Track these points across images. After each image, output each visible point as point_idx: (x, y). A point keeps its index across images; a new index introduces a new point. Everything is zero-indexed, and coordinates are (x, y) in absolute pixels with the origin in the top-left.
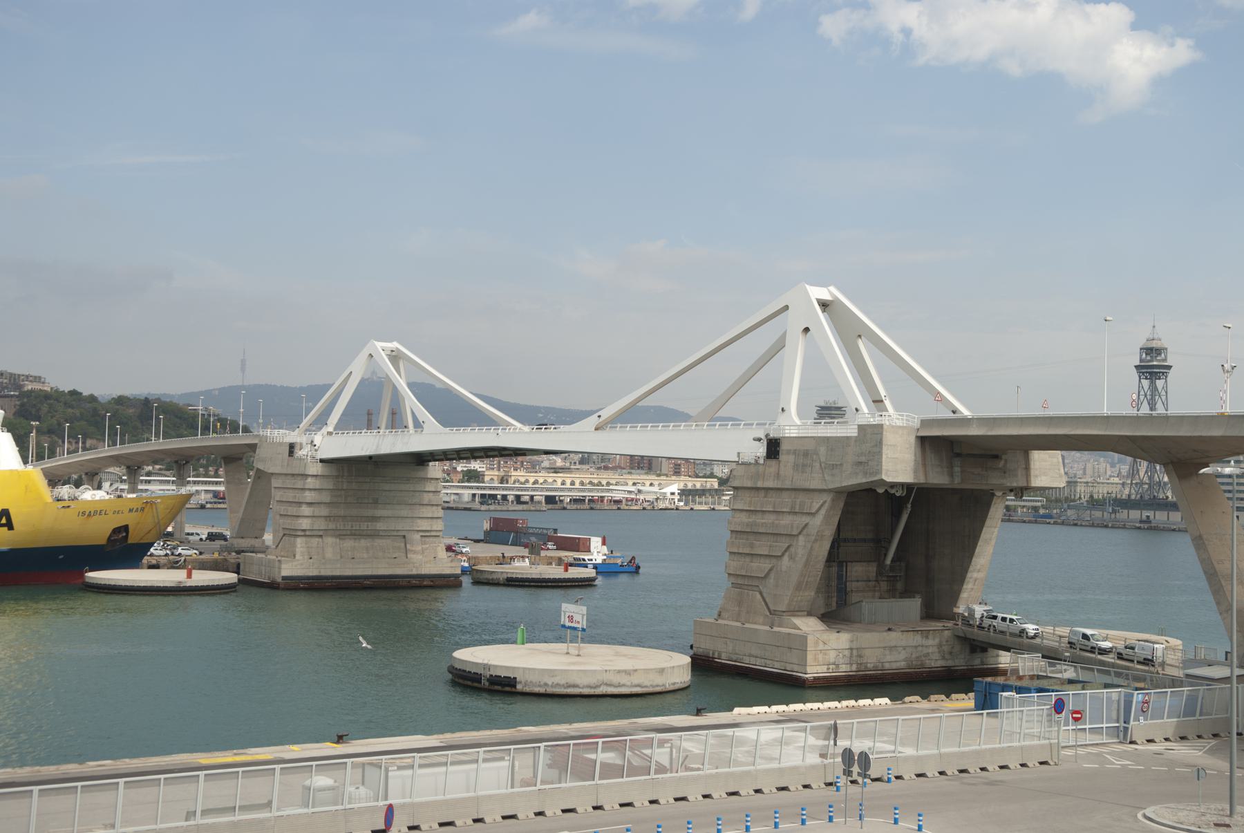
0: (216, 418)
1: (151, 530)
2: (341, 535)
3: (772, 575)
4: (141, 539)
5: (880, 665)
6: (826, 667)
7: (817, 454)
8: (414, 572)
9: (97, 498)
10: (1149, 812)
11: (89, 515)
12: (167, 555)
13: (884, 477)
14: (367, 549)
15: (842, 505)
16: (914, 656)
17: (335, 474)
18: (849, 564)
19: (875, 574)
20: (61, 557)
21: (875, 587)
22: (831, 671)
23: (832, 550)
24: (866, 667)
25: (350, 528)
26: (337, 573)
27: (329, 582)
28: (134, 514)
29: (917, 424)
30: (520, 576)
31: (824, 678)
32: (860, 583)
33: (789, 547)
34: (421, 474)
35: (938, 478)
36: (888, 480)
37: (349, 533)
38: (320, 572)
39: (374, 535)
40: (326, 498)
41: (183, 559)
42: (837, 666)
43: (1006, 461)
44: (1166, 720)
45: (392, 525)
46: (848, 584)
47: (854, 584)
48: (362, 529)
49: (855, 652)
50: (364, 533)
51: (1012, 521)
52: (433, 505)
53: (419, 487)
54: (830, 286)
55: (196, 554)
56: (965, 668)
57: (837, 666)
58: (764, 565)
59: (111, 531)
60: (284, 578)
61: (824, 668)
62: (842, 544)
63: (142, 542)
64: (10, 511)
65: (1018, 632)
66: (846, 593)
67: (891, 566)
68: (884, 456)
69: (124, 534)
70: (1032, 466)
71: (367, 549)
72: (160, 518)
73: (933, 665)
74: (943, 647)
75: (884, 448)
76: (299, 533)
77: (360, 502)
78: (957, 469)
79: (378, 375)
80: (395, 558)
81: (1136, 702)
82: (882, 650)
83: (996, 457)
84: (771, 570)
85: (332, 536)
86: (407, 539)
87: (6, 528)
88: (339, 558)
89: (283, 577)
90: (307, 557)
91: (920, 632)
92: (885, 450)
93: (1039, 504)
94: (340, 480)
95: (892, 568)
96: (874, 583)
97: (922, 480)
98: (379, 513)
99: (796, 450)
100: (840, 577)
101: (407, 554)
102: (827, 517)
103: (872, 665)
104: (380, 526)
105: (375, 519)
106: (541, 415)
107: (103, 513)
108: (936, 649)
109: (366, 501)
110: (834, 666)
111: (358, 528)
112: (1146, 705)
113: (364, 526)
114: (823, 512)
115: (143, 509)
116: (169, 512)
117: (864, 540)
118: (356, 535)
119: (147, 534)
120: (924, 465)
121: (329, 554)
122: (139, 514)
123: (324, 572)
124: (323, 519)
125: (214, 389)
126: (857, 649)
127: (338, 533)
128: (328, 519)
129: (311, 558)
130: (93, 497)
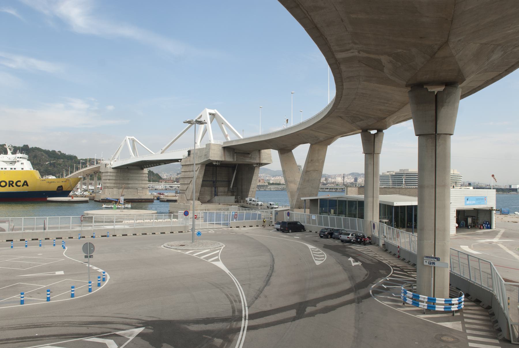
2: (119, 188)
3: (188, 189)
4: (67, 189)
7: (198, 154)
8: (140, 198)
9: (53, 178)
10: (165, 245)
11: (50, 183)
12: (81, 195)
14: (126, 192)
15: (204, 168)
17: (116, 172)
19: (227, 191)
20: (44, 194)
23: (380, 217)
28: (63, 183)
29: (222, 144)
30: (170, 199)
33: (191, 181)
34: (141, 172)
35: (229, 159)
36: (212, 159)
39: (128, 188)
40: (114, 178)
41: (85, 196)
43: (252, 155)
44: (244, 221)
45: (133, 185)
46: (218, 193)
47: (220, 193)
51: (337, 192)
52: (145, 180)
53: (141, 175)
54: (215, 109)
58: (185, 187)
60: (102, 199)
62: (217, 182)
64: (27, 181)
67: (232, 188)
68: (210, 152)
69: (61, 188)
70: (261, 157)
71: (126, 192)
72: (71, 184)
75: (211, 150)
76: (106, 187)
78: (235, 157)
81: (232, 215)
83: (249, 154)
84: (187, 188)
85: (116, 188)
87: (26, 186)
93: (343, 187)
95: (233, 188)
97: (223, 159)
98: (129, 182)
100: (215, 191)
102: (200, 172)
104: (130, 186)
105: (128, 184)
112: (236, 216)
114: (198, 170)
115: (66, 181)
117: (224, 181)
120: (224, 155)
121: (115, 193)
122: (65, 183)
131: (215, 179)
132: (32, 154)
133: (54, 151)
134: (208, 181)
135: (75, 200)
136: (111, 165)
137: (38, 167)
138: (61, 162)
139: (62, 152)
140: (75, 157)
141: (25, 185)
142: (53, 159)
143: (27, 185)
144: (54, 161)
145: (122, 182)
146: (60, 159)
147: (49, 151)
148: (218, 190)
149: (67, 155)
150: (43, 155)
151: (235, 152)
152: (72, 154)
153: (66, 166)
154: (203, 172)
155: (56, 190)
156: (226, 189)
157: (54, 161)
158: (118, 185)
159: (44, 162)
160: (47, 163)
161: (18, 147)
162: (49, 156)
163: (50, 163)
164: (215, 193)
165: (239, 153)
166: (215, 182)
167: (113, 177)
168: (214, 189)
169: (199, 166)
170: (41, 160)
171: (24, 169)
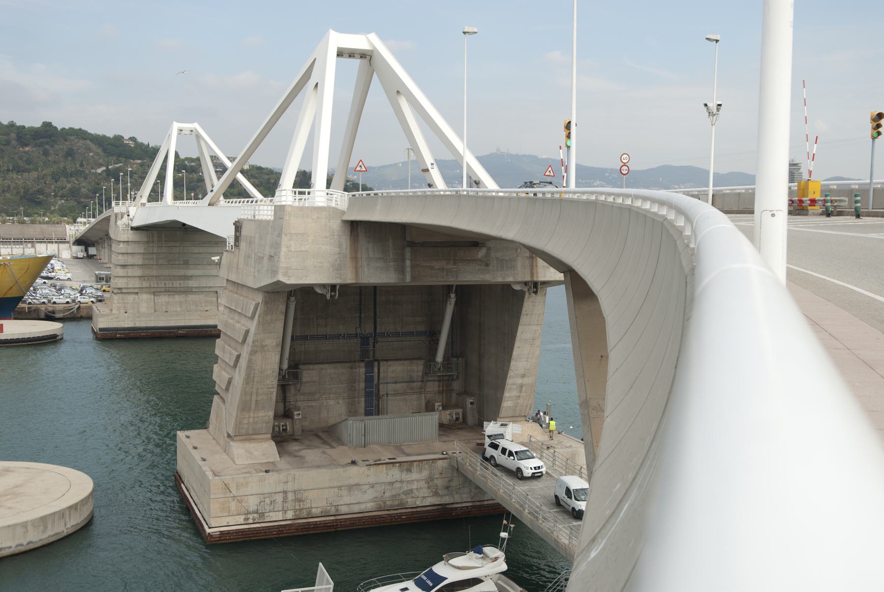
0: (351, 183)
1: (11, 288)
5: (333, 509)
6: (243, 517)
12: (68, 303)
14: (181, 303)
16: (388, 494)
17: (145, 239)
18: (381, 363)
19: (420, 374)
21: (421, 388)
22: (251, 521)
24: (310, 512)
25: (163, 286)
26: (152, 324)
31: (237, 532)
32: (399, 385)
36: (288, 282)
37: (163, 290)
38: (135, 324)
39: (187, 291)
40: (138, 260)
41: (77, 306)
42: (262, 515)
43: (489, 249)
45: (204, 283)
46: (381, 386)
47: (391, 387)
48: (174, 286)
49: (290, 496)
50: (178, 290)
54: (369, 33)
55: (92, 302)
56: (470, 504)
57: (262, 515)
61: (241, 519)
62: (380, 339)
63: (5, 297)
65: (514, 470)
66: (378, 397)
68: (284, 249)
73: (418, 503)
74: (435, 481)
77: (171, 263)
78: (408, 263)
79: (501, 151)
80: (207, 311)
82: (336, 490)
85: (147, 293)
86: (218, 294)
88: (153, 311)
89: (99, 328)
90: (123, 311)
91: (398, 465)
94: (151, 245)
96: (420, 383)
97: (348, 278)
98: (190, 272)
100: (369, 380)
103: (319, 510)
104: (192, 283)
105: (186, 278)
106: (607, 174)
108: (423, 484)
109: (177, 263)
110: (255, 515)
111: (172, 286)
113: (177, 284)
117: (411, 334)
119: (9, 290)
120: (355, 258)
121: (143, 308)
123: (139, 324)
124: (137, 278)
126: (295, 492)
127: (153, 290)
128: (142, 278)
129: (126, 312)
131: (368, 329)
132: (61, 147)
134: (338, 336)
136: (131, 217)
137: (78, 181)
139: (140, 140)
142: (115, 158)
145: (166, 272)
146: (134, 160)
148: (382, 375)
149: (152, 147)
150: (90, 150)
151: (408, 239)
156: (414, 368)
158: (154, 284)
159: (93, 168)
160: (99, 171)
161: (29, 127)
162: (105, 150)
163: (108, 170)
164: (366, 388)
165: (424, 244)
166: (371, 341)
167: (137, 256)
168: (362, 370)
169: (259, 298)
170: (84, 163)
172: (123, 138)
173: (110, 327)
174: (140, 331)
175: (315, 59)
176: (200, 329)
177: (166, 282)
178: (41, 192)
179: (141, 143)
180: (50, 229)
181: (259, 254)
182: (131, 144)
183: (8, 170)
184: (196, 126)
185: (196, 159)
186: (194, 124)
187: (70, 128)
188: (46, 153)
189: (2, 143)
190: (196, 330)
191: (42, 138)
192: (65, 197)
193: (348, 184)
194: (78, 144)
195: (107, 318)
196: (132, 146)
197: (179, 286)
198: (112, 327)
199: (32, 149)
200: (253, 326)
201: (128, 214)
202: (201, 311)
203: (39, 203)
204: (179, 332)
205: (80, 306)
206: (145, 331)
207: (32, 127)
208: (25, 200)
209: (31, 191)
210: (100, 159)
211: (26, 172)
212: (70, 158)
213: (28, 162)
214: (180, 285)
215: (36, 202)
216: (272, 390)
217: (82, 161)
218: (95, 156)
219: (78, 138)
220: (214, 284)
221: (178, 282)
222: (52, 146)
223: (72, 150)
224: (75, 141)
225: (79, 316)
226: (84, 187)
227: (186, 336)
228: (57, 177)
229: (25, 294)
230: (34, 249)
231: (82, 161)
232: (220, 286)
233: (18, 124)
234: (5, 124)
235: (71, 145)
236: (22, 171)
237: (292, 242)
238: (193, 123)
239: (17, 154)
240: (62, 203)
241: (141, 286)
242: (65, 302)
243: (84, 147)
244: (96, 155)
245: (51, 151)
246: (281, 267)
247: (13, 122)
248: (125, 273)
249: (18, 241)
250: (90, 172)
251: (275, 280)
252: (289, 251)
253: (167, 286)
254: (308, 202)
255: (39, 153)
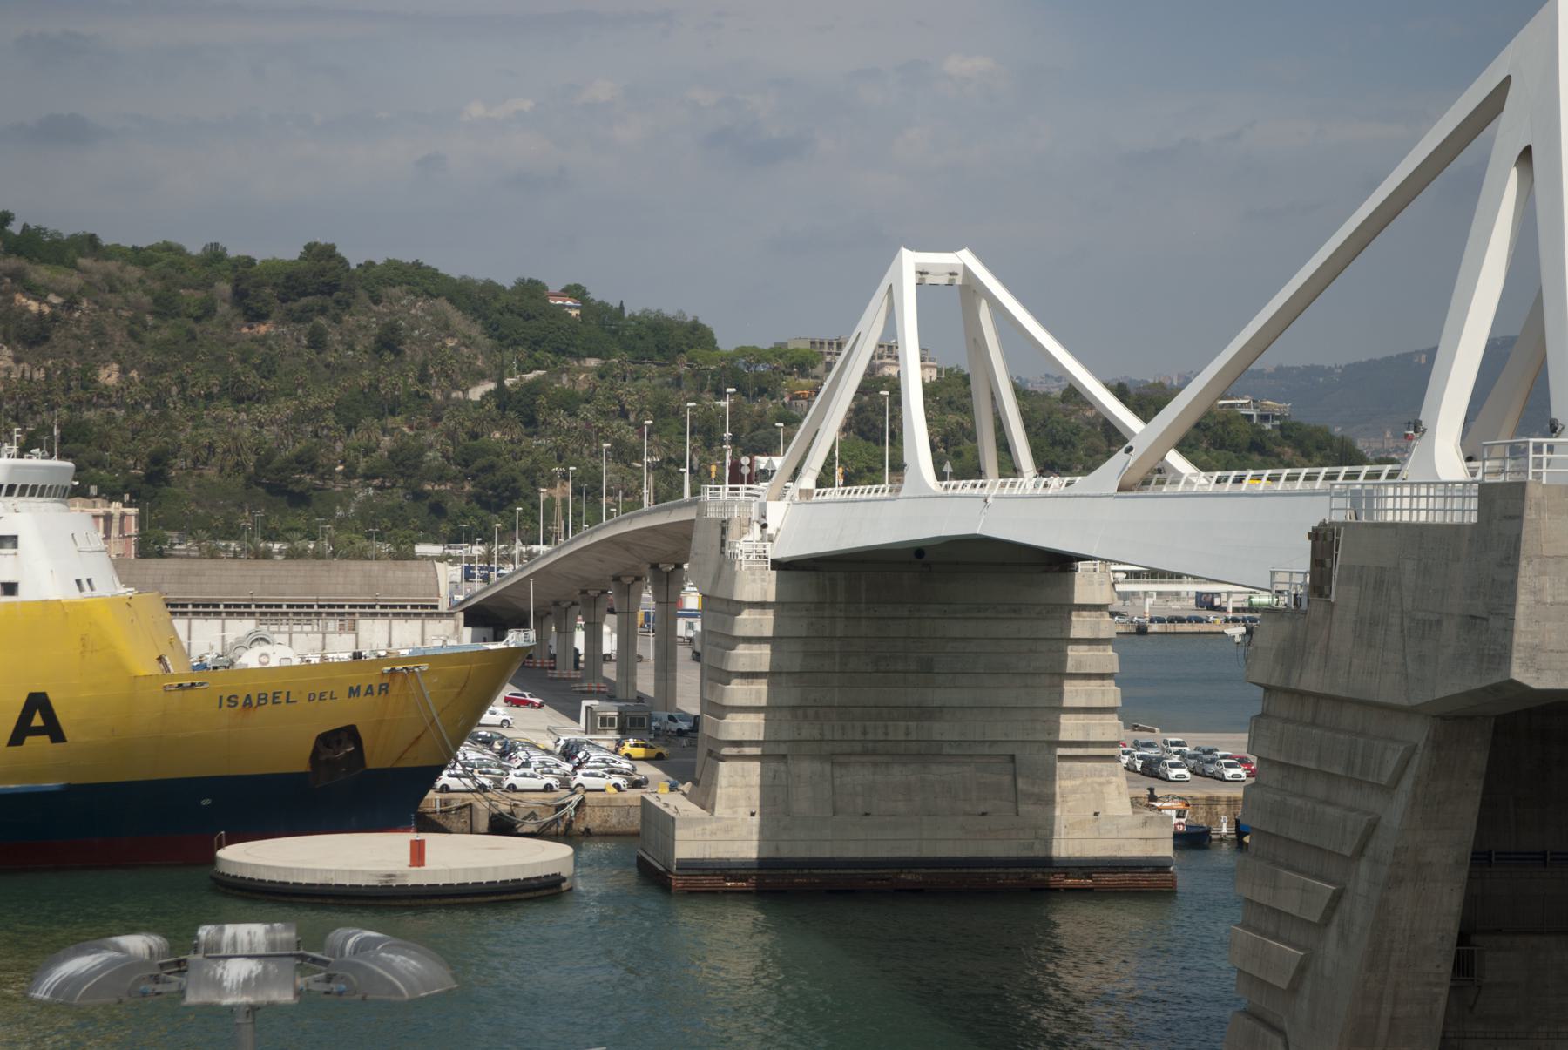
0: (1277, 423)
1: (418, 738)
2: (835, 758)
9: (274, 663)
12: (548, 788)
13: (1520, 673)
15: (1479, 760)
20: (206, 802)
25: (858, 736)
26: (825, 852)
27: (803, 876)
28: (362, 700)
33: (1337, 898)
36: (1536, 685)
37: (858, 747)
38: (777, 849)
39: (928, 754)
41: (576, 799)
48: (889, 738)
55: (617, 786)
59: (312, 742)
64: (51, 697)
80: (983, 814)
85: (813, 756)
87: (45, 739)
92: (1527, 574)
98: (937, 697)
99: (1363, 567)
101: (1016, 802)
104: (942, 730)
105: (925, 713)
107: (283, 698)
113: (898, 731)
114: (1407, 783)
115: (385, 689)
116: (459, 694)
118: (878, 753)
125: (1417, 352)
128: (800, 713)
130: (264, 659)
132: (363, 320)
133: (537, 283)
135: (441, 881)
136: (770, 530)
138: (583, 382)
139: (596, 294)
140: (698, 335)
141: (38, 731)
143: (53, 730)
144: (529, 376)
146: (579, 357)
147: (491, 288)
149: (633, 317)
152: (670, 311)
153: (624, 414)
154: (1468, 810)
155: (301, 765)
157: (529, 376)
159: (456, 387)
160: (476, 394)
162: (493, 329)
169: (1418, 732)
171: (21, 589)
172: (545, 288)
173: (707, 857)
174: (793, 872)
175: (1508, 79)
176: (965, 871)
177: (868, 723)
178: (306, 462)
179: (601, 303)
180: (390, 574)
181: (1420, 615)
182: (570, 307)
183: (209, 397)
184: (965, 258)
185: (772, 350)
186: (958, 253)
187: (389, 261)
188: (317, 342)
189: (191, 310)
190: (951, 871)
191: (305, 294)
192: (375, 477)
193: (1268, 426)
194: (413, 311)
195: (699, 828)
196: (574, 313)
197: (903, 738)
198: (713, 856)
199: (276, 328)
200: (1394, 812)
201: (763, 521)
202: (967, 814)
203: (300, 499)
204: (903, 876)
205: (584, 799)
206: (806, 871)
207: (274, 259)
208: (260, 489)
209: (277, 461)
210: (476, 357)
211: (258, 401)
212: (389, 357)
213: (267, 369)
214: (907, 734)
215: (291, 494)
216: (1436, 990)
217: (424, 366)
218: (463, 348)
219: (413, 293)
220: (1006, 735)
221: (902, 724)
222: (337, 320)
223: (393, 329)
224: (405, 302)
225: (582, 829)
226: (431, 446)
227: (921, 890)
228: (352, 415)
229: (446, 758)
230: (354, 636)
231: (424, 366)
232: (1026, 738)
233: (232, 253)
234: (194, 253)
235: (392, 313)
236: (249, 399)
237: (1545, 578)
238: (959, 250)
239: (233, 345)
240: (369, 498)
241: (798, 738)
242: (542, 787)
243: (429, 319)
244: (464, 344)
245: (334, 336)
246: (1518, 645)
247: (216, 245)
248: (753, 696)
249: (303, 611)
250: (448, 397)
251: (1496, 679)
252: (1538, 602)
253: (870, 737)
254: (1548, 473)
255: (298, 341)
